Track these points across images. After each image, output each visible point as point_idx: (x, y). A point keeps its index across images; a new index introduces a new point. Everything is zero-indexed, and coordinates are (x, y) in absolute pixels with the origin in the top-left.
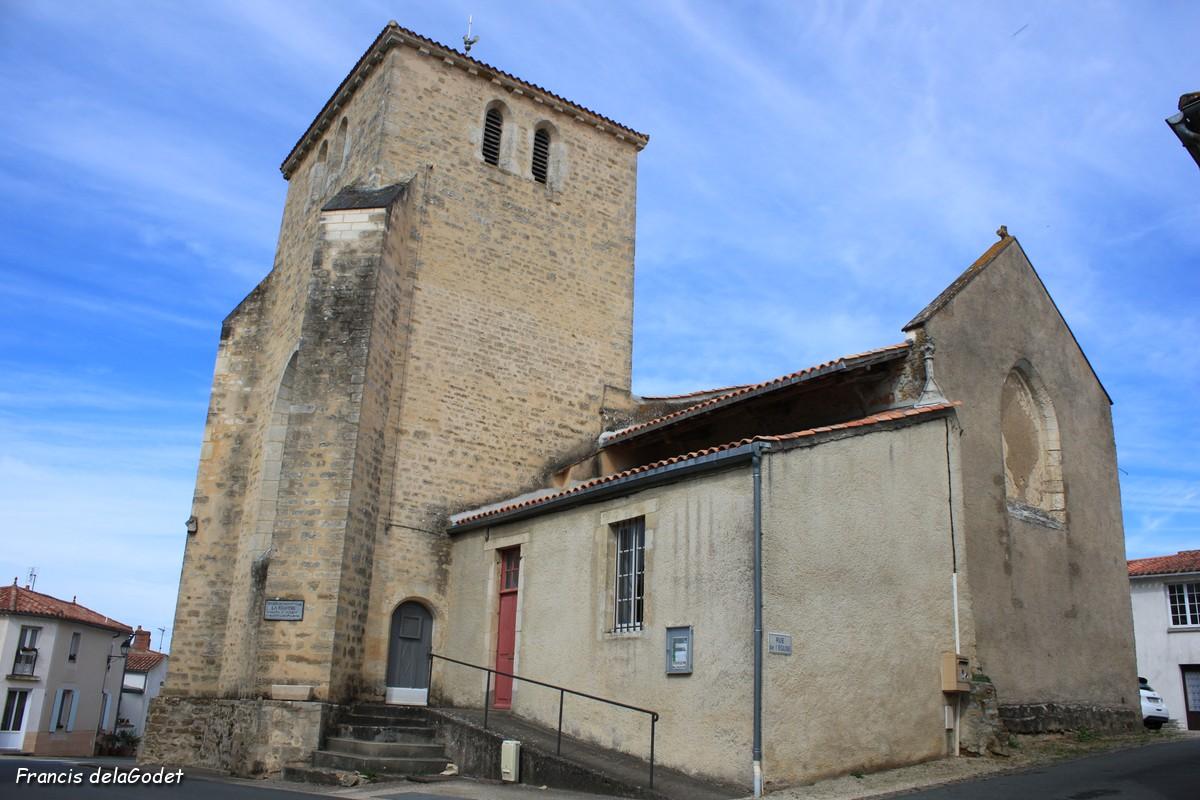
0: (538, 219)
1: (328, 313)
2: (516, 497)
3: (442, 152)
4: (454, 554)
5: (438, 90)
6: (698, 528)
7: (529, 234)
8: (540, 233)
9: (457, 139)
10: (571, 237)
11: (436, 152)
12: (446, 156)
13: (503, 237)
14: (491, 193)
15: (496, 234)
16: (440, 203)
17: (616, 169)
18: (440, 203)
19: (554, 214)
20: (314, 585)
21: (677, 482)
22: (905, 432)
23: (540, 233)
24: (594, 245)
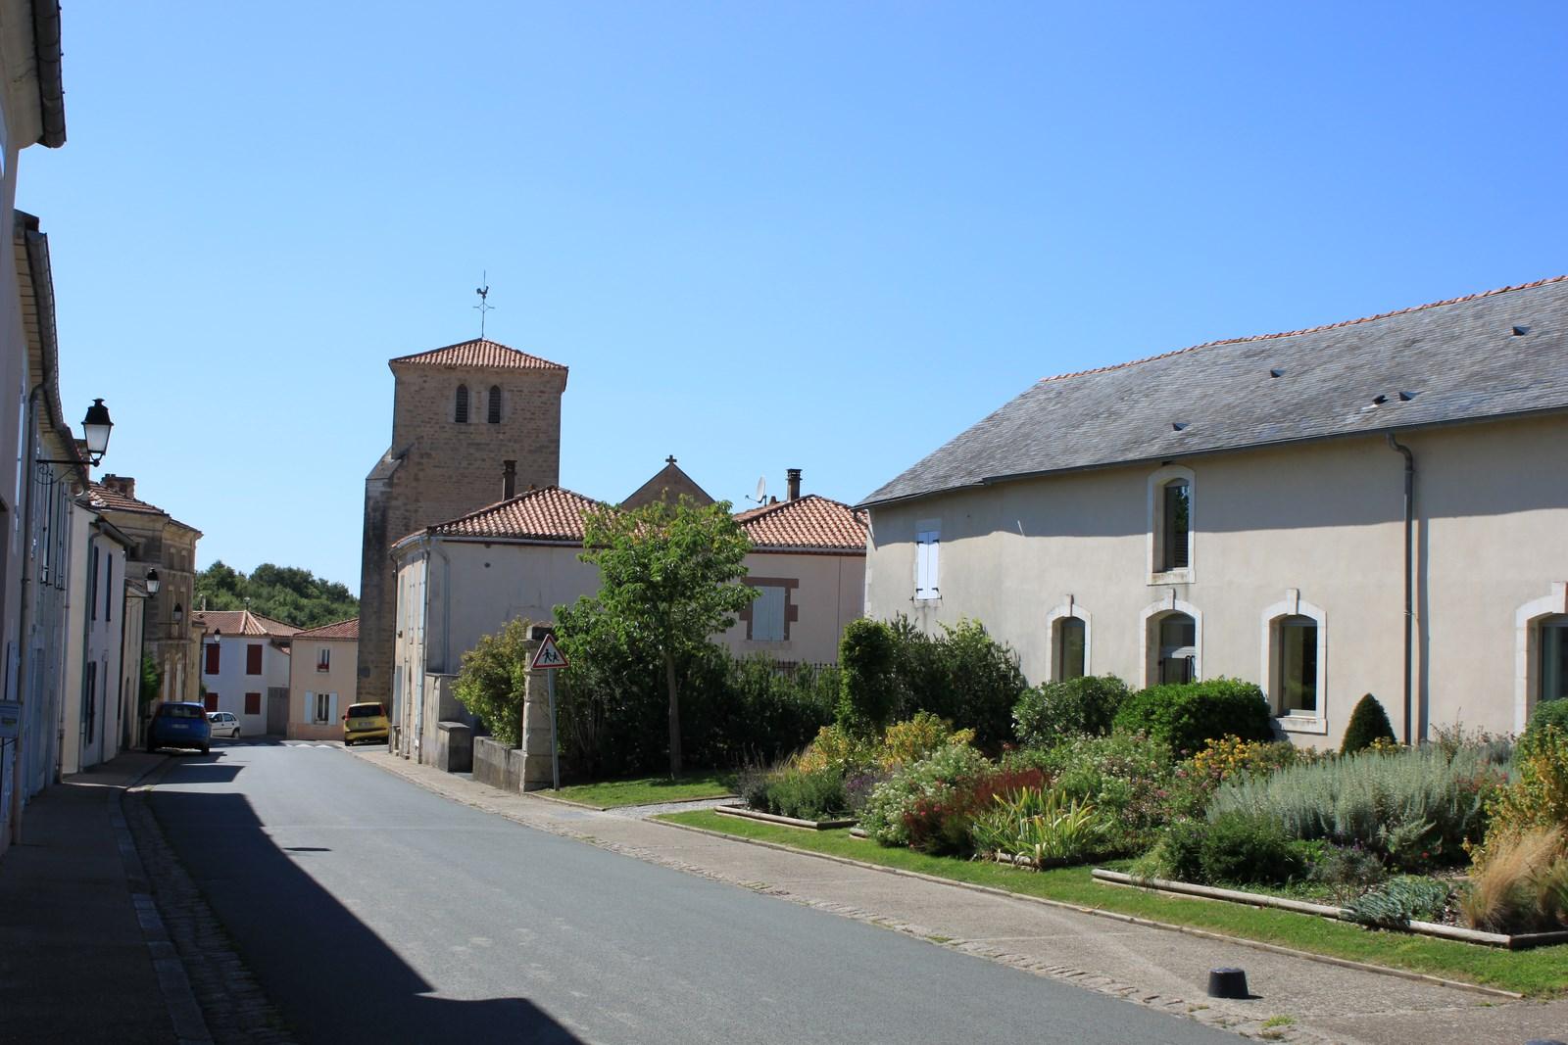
0: (491, 446)
1: (371, 534)
2: (1410, 453)
3: (429, 425)
4: (1299, 748)
5: (423, 389)
6: (20, 655)
7: (485, 457)
8: (492, 455)
9: (436, 414)
10: (514, 451)
11: (425, 427)
12: (431, 427)
13: (469, 464)
14: (459, 440)
15: (465, 464)
16: (429, 455)
17: (545, 397)
18: (429, 455)
19: (502, 440)
20: (372, 662)
21: (53, 695)
22: (336, 643)
23: (492, 455)
24: (530, 451)
